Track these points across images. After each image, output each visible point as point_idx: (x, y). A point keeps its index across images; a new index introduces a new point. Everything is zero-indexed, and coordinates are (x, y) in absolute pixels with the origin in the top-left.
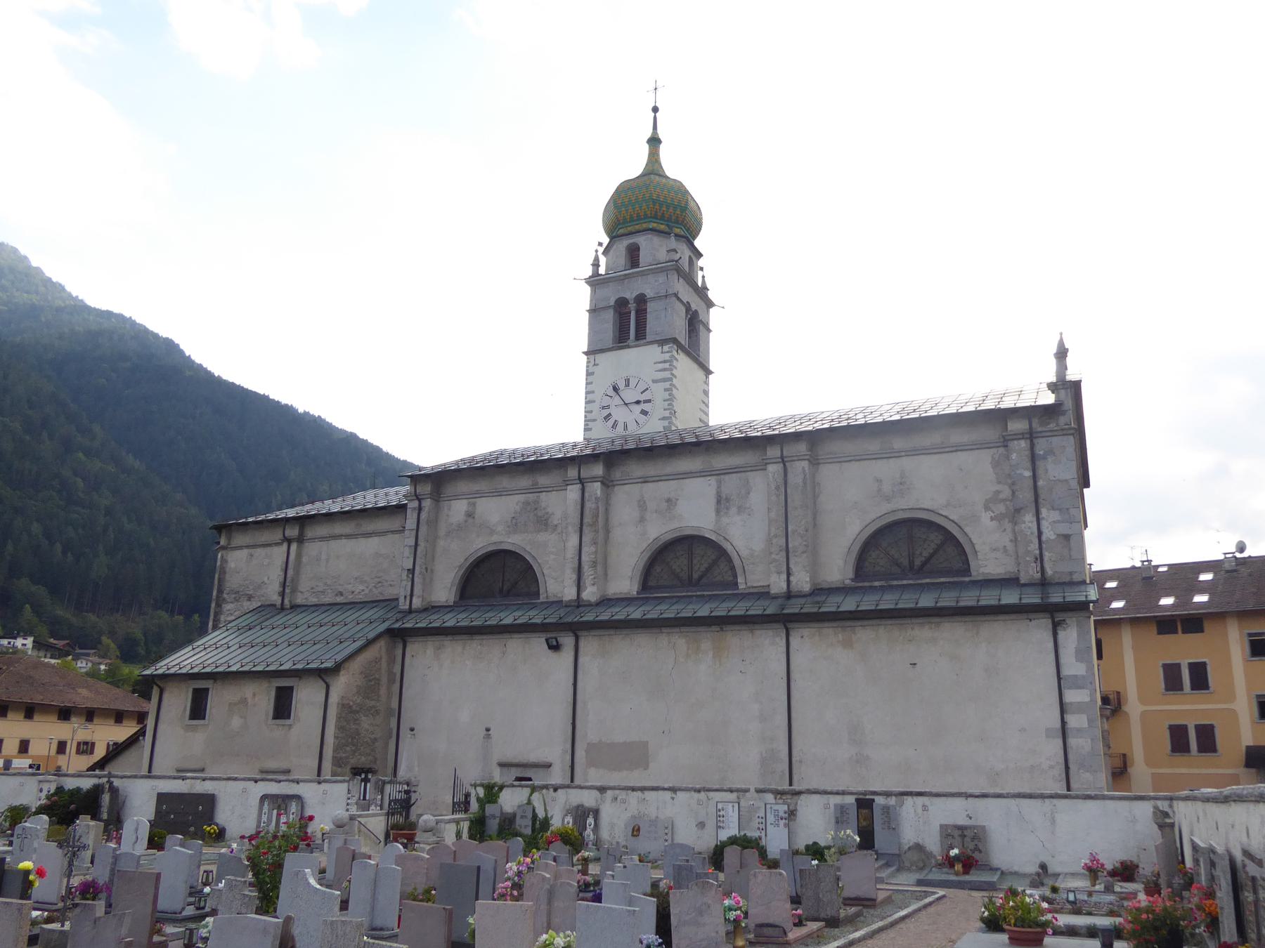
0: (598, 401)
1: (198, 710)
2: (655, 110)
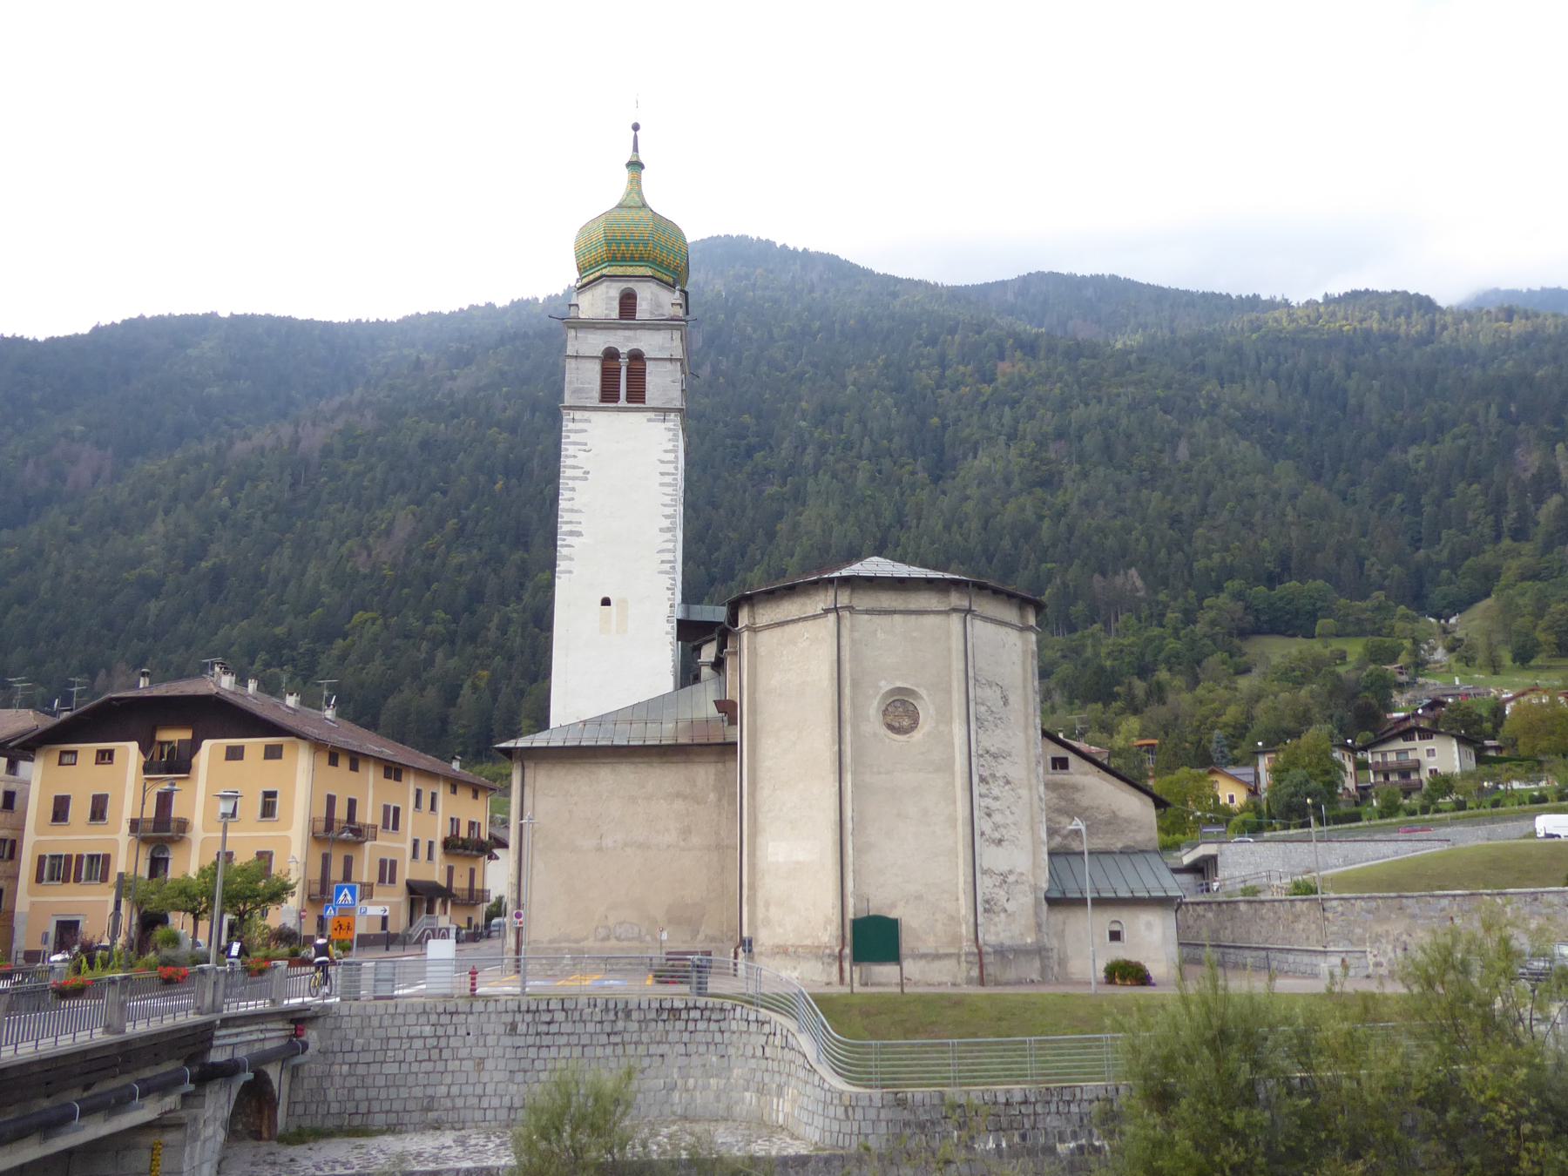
2: (636, 127)
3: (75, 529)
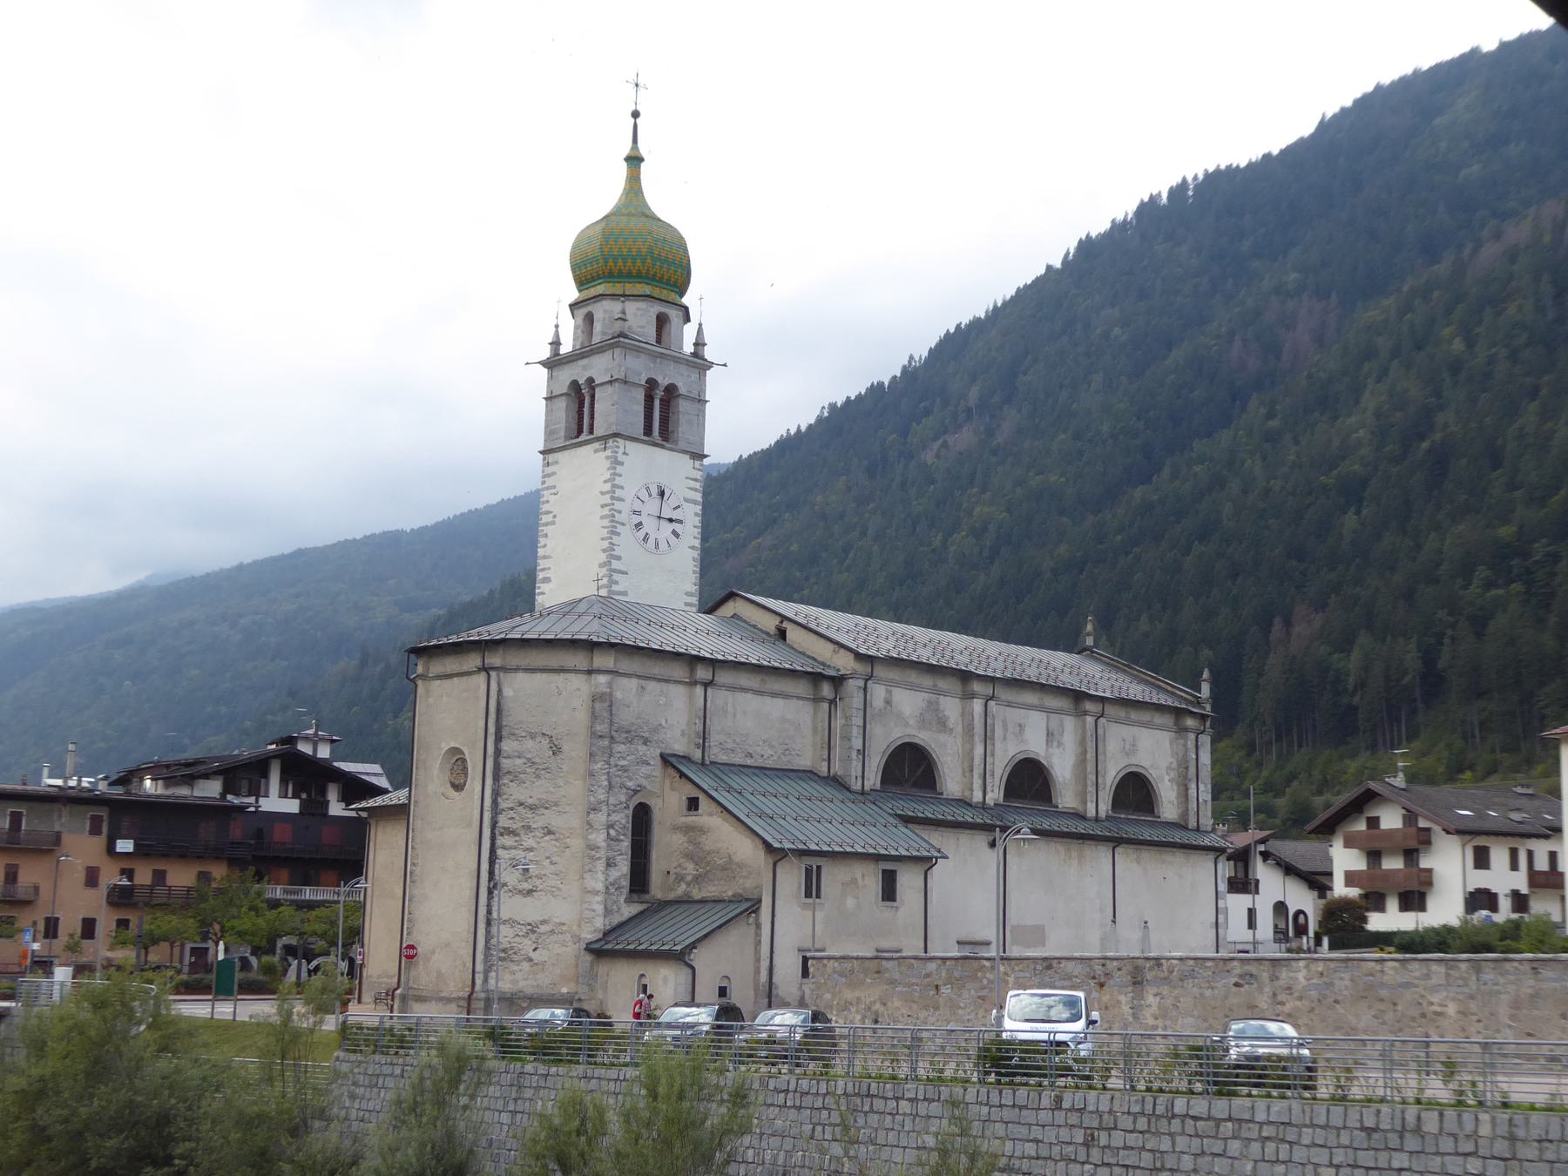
0: (629, 500)
1: (812, 888)
2: (636, 115)
3: (1274, 424)
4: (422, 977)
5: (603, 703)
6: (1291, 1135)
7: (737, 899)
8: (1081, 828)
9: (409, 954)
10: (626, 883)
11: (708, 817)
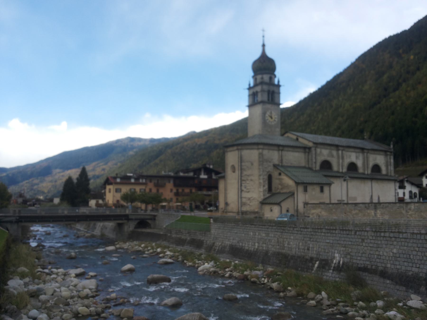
1: (305, 190)
4: (229, 208)
5: (261, 155)
6: (408, 240)
7: (290, 192)
8: (364, 176)
9: (227, 204)
10: (267, 190)
11: (284, 177)
